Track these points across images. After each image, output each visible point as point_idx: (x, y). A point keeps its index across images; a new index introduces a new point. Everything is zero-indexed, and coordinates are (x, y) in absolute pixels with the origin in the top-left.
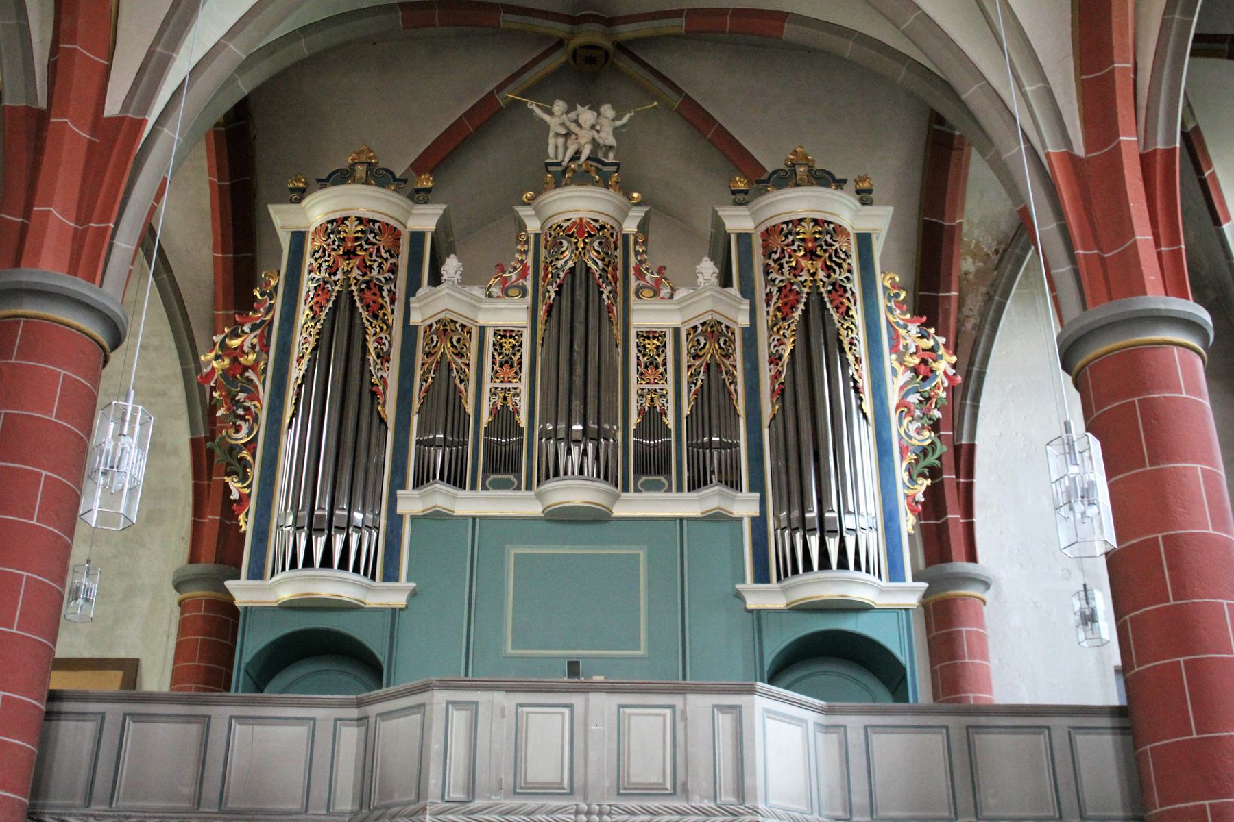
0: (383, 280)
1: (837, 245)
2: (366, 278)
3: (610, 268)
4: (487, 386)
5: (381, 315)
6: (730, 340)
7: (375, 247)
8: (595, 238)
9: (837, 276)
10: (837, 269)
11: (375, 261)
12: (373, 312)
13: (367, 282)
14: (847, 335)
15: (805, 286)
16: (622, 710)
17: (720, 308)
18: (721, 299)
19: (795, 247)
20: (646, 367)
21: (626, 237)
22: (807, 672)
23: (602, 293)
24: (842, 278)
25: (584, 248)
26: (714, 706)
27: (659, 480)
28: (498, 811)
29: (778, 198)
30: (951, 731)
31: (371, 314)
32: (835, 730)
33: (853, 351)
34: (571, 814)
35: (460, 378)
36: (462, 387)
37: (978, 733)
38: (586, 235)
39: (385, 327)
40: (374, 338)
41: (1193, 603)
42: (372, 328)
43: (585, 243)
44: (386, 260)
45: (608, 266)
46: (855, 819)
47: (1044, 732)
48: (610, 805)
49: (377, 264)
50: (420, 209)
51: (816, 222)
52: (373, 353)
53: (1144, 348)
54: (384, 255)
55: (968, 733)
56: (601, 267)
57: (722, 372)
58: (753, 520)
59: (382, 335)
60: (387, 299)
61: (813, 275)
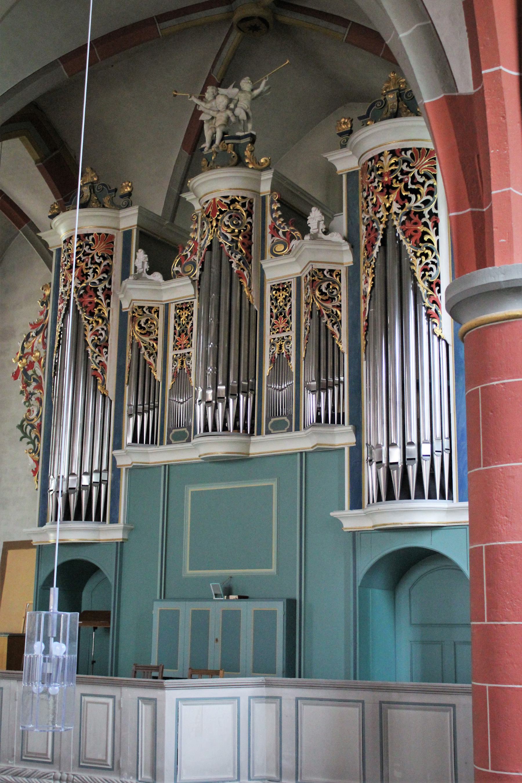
0: (97, 282)
1: (415, 171)
2: (84, 285)
3: (240, 238)
4: (171, 353)
5: (96, 312)
6: (334, 282)
7: (90, 256)
8: (225, 214)
9: (412, 204)
10: (413, 197)
11: (90, 268)
12: (90, 312)
13: (84, 288)
14: (421, 262)
15: (381, 223)
16: (83, 698)
17: (322, 257)
18: (318, 249)
19: (375, 184)
20: (277, 318)
21: (264, 198)
22: (433, 567)
23: (232, 262)
24: (418, 204)
25: (216, 226)
26: (139, 698)
27: (284, 420)
28: (11, 773)
29: (367, 134)
30: (366, 705)
31: (88, 314)
32: (273, 700)
33: (427, 277)
34: (51, 779)
35: (149, 352)
36: (151, 360)
37: (390, 708)
38: (218, 213)
39: (100, 321)
40: (91, 332)
41: (502, 625)
42: (89, 324)
43: (217, 220)
44: (100, 264)
45: (238, 236)
46: (283, 781)
47: (450, 710)
48: (74, 775)
49: (91, 270)
50: (124, 213)
51: (393, 153)
52: (91, 345)
53: (491, 326)
54: (98, 261)
55: (381, 708)
56: (230, 239)
57: (323, 315)
58: (351, 448)
59: (99, 328)
60: (102, 297)
61: (388, 209)
